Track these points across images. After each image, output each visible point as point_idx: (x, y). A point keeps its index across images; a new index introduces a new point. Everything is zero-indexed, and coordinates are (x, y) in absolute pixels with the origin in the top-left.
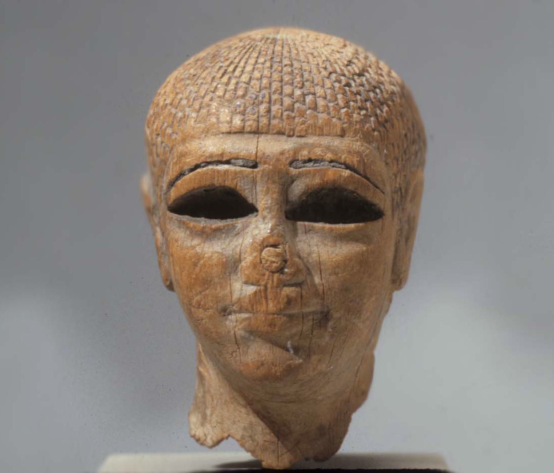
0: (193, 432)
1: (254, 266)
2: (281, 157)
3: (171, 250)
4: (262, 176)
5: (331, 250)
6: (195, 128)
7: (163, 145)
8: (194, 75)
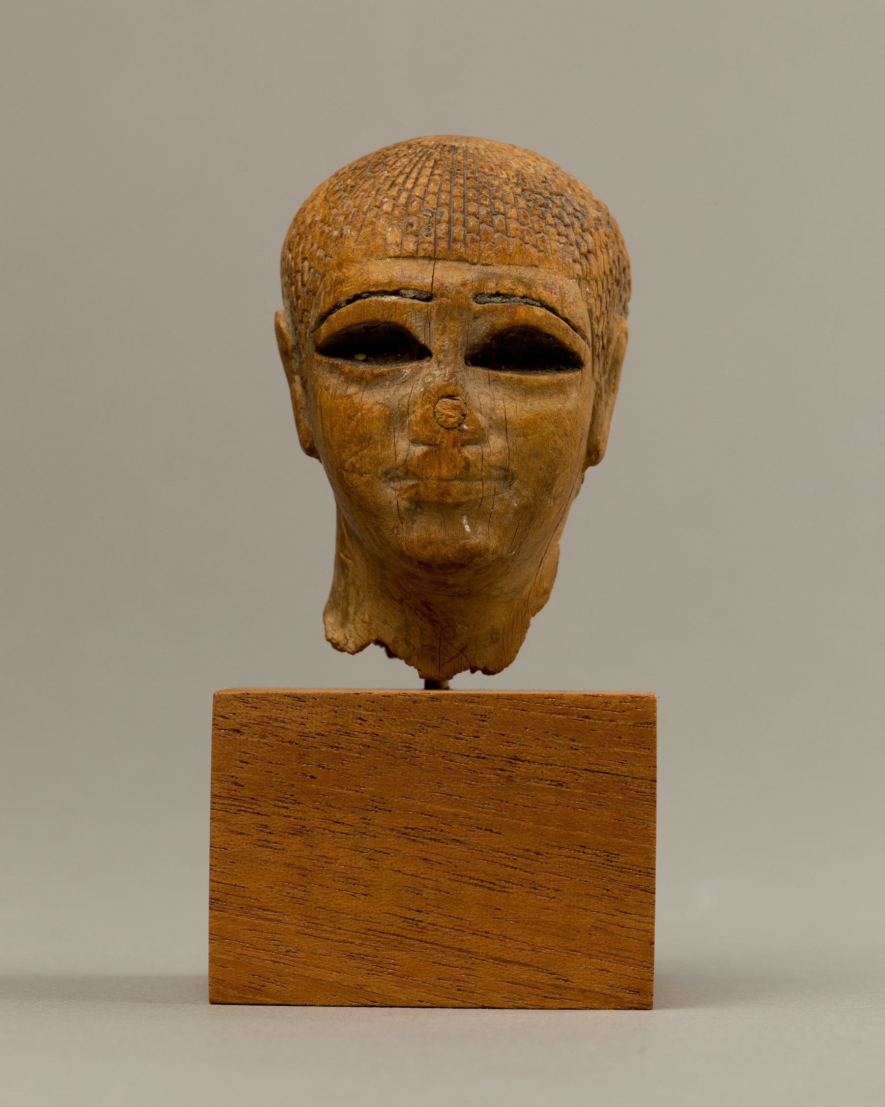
0: (330, 636)
1: (425, 420)
2: (462, 289)
3: (318, 401)
4: (438, 312)
5: (520, 405)
6: (355, 251)
7: (312, 270)
8: (352, 187)
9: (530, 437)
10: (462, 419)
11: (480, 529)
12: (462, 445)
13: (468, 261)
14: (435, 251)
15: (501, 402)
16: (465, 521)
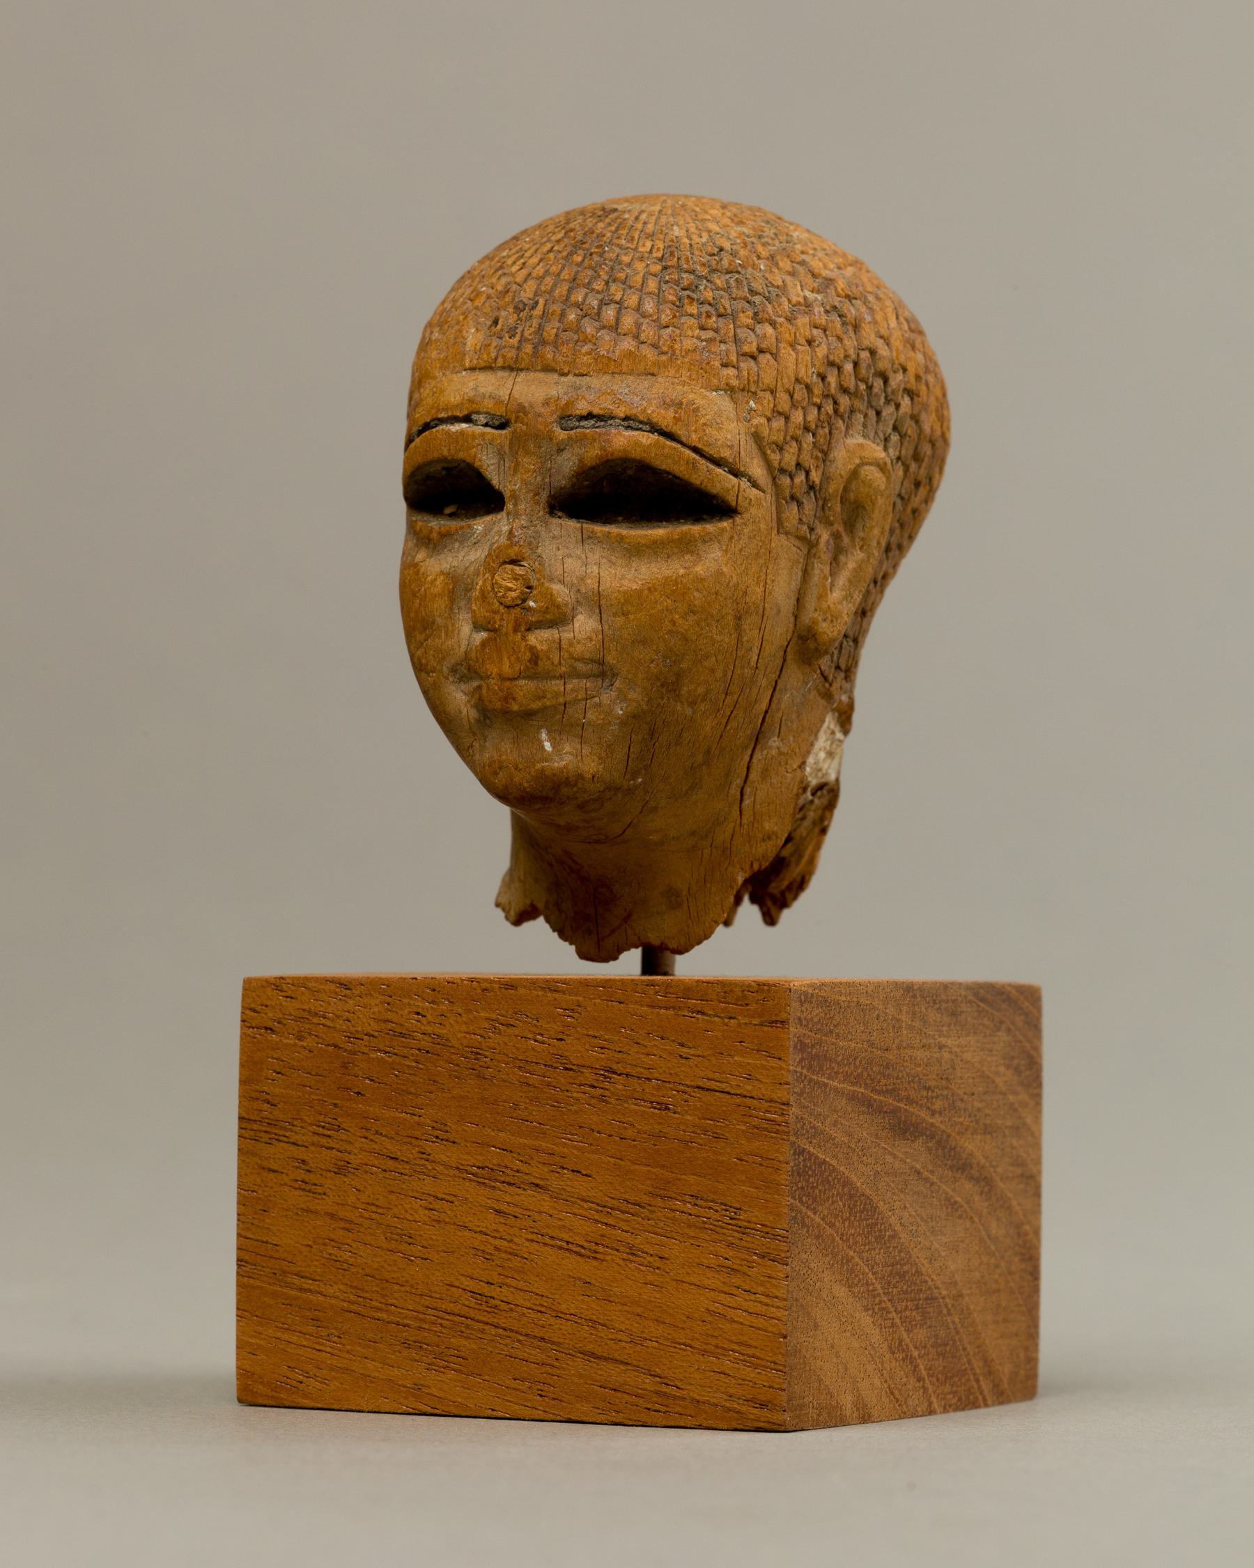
9: (631, 617)
10: (526, 593)
11: (567, 748)
12: (529, 630)
13: (556, 371)
14: (517, 358)
15: (595, 568)
16: (544, 736)
